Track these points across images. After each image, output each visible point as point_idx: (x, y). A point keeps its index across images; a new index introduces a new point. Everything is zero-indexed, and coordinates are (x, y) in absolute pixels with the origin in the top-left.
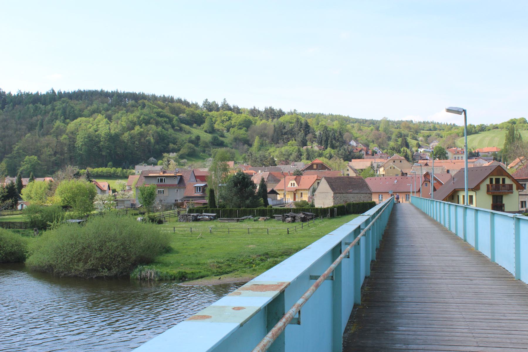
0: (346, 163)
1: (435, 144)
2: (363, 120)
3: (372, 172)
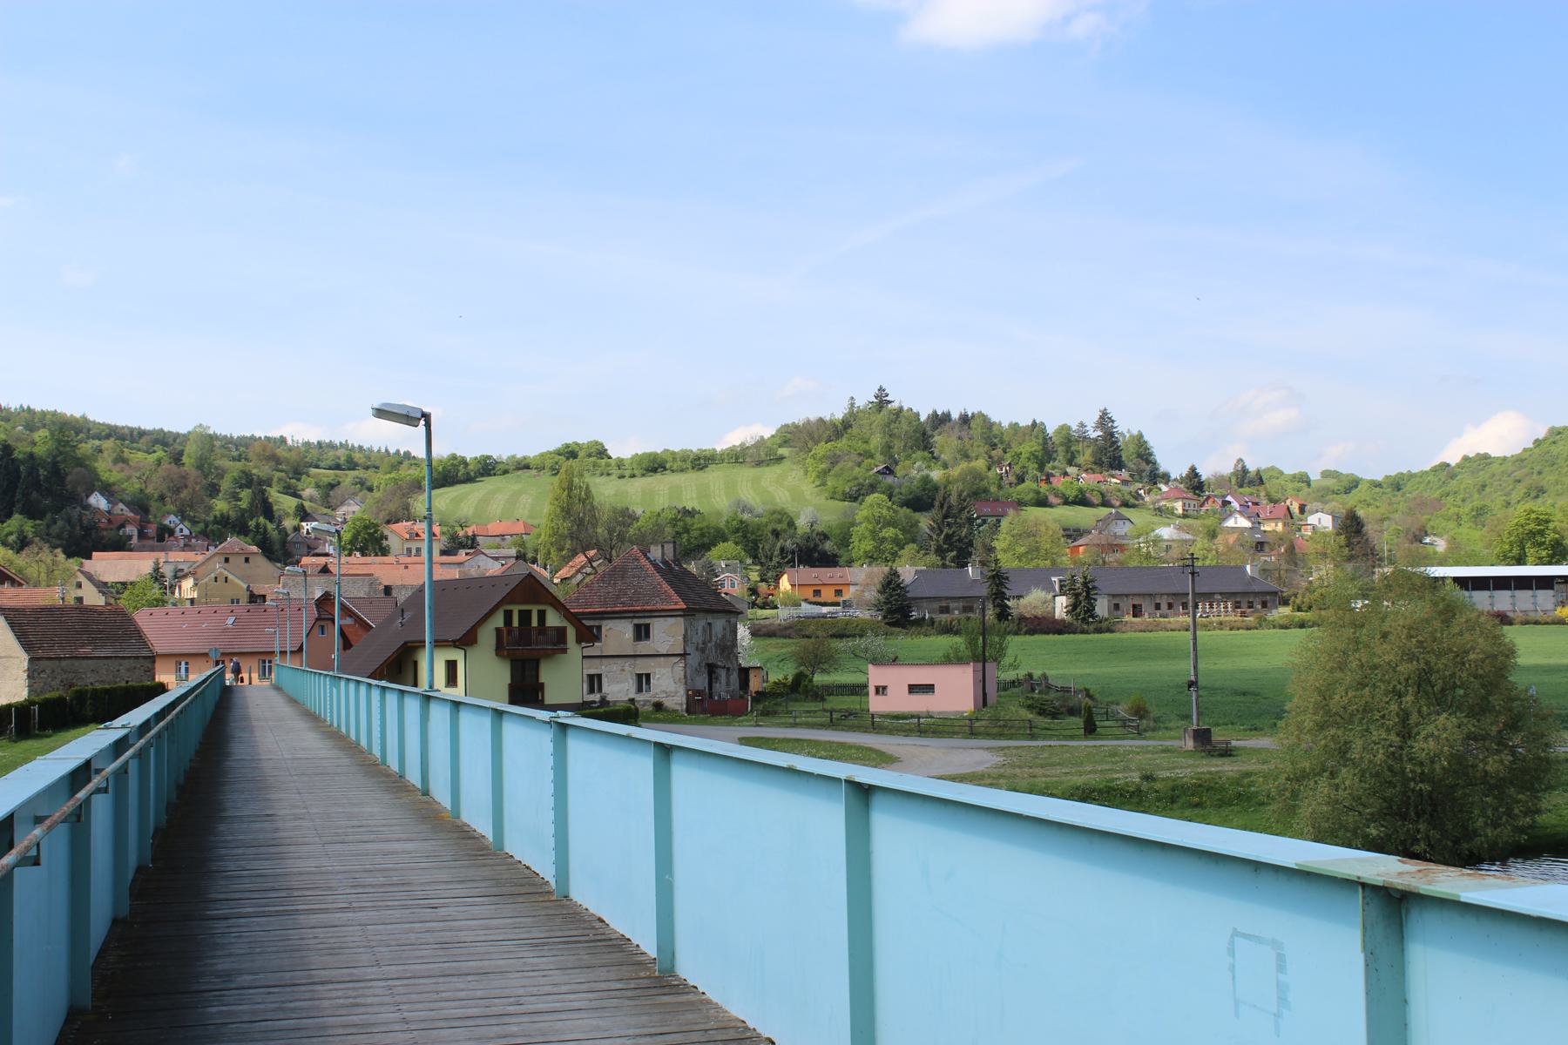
0: (73, 564)
1: (352, 510)
2: (132, 430)
3: (156, 592)
